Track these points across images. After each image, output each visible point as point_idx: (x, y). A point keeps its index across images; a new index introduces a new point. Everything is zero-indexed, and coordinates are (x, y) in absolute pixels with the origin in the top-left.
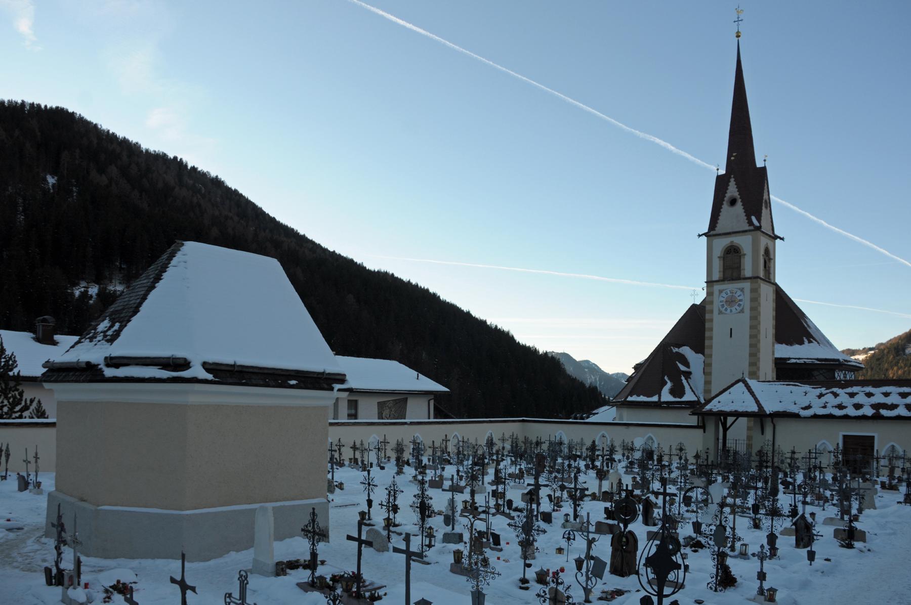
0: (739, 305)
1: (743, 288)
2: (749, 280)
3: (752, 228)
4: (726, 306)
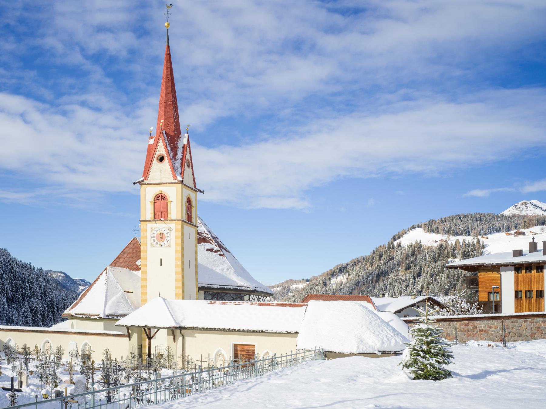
0: (167, 241)
1: (151, 228)
3: (176, 181)
4: (156, 241)
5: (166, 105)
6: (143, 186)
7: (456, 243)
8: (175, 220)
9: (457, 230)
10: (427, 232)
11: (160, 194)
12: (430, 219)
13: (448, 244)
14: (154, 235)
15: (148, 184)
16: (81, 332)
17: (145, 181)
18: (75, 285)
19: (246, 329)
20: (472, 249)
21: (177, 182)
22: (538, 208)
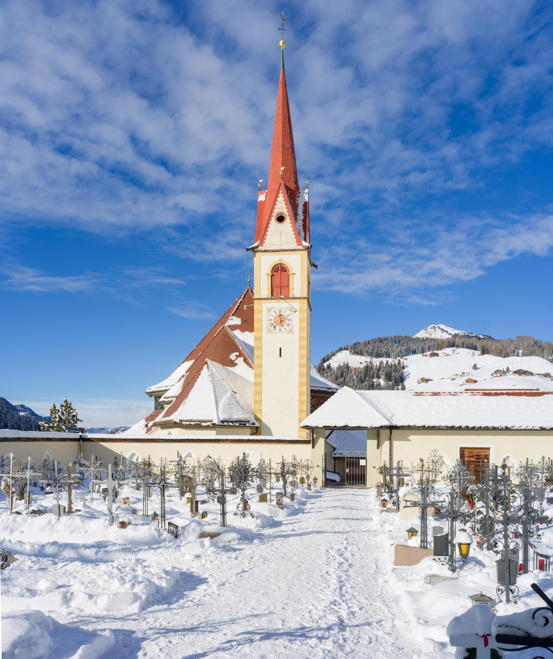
0: (288, 325)
1: (268, 308)
2: (298, 300)
3: (301, 247)
5: (284, 149)
6: (258, 254)
7: (380, 364)
8: (299, 298)
9: (379, 352)
10: (352, 354)
11: (279, 264)
12: (355, 341)
13: (373, 365)
14: (271, 318)
15: (265, 251)
16: (243, 440)
17: (259, 247)
18: (15, 411)
19: (483, 425)
20: (394, 370)
21: (302, 248)
22: (444, 332)
